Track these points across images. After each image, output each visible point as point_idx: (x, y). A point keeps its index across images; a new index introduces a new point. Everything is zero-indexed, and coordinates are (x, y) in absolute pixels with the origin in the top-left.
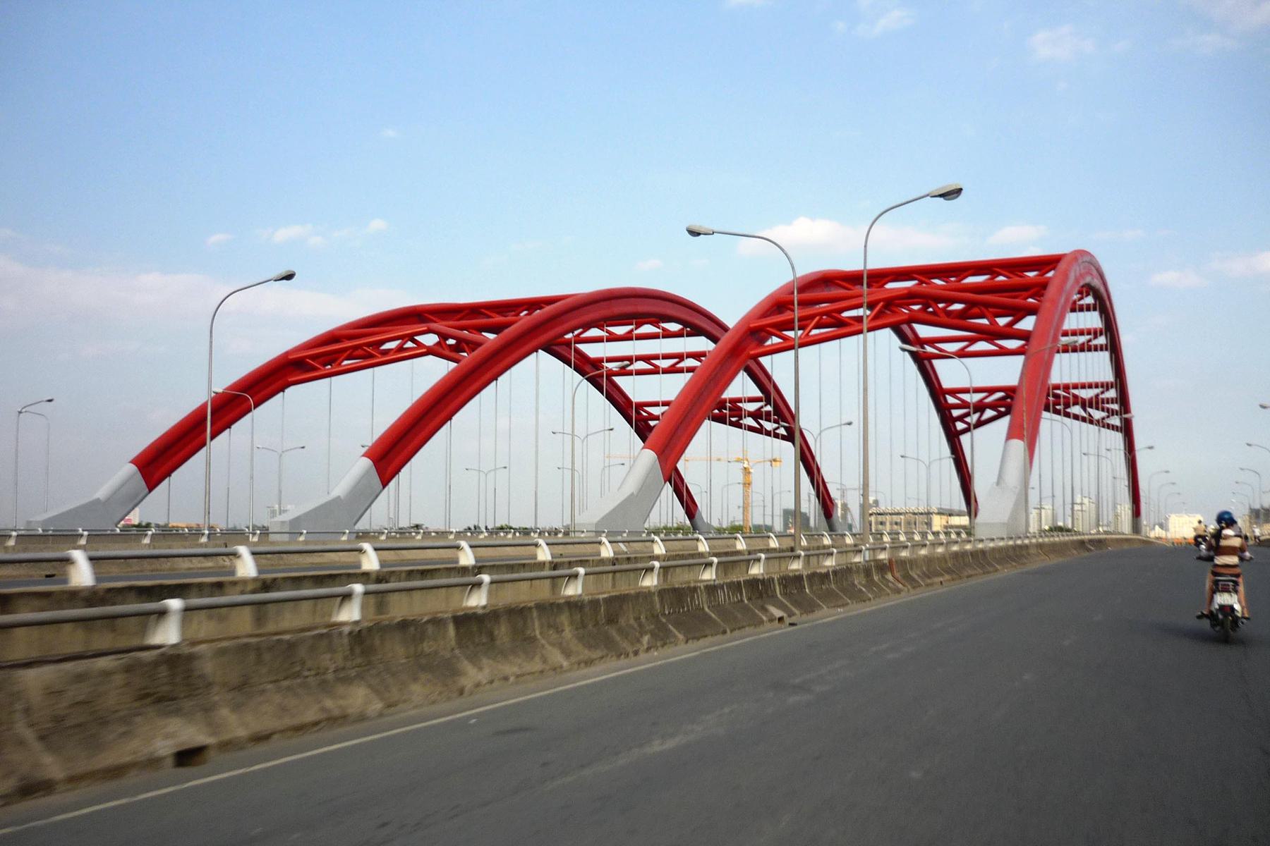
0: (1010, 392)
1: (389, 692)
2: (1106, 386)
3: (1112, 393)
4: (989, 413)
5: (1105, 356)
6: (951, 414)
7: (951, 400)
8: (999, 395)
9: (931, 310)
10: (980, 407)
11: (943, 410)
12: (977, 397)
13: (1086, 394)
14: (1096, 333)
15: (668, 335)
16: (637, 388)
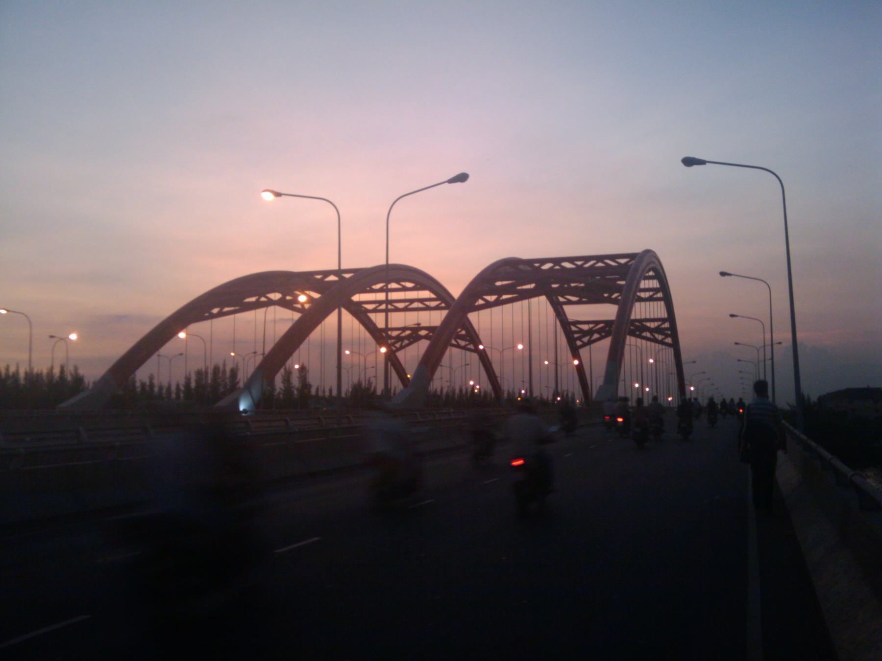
0: (608, 323)
2: (663, 320)
3: (667, 325)
4: (596, 336)
5: (662, 304)
7: (573, 328)
8: (408, 332)
10: (590, 332)
11: (569, 334)
12: (656, 324)
13: (652, 325)
14: (656, 290)
15: (405, 289)
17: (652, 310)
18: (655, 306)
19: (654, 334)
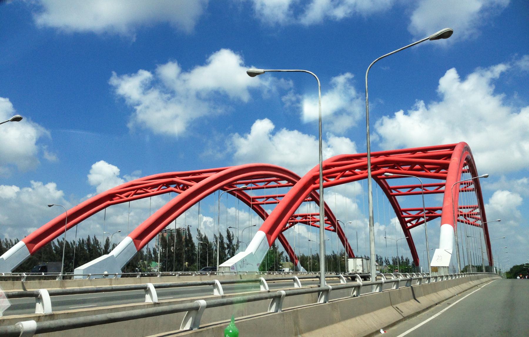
1: (499, 328)
3: (478, 210)
6: (405, 220)
7: (405, 214)
9: (396, 167)
10: (417, 218)
16: (403, 202)
17: (480, 260)
18: (476, 262)
19: (440, 172)
